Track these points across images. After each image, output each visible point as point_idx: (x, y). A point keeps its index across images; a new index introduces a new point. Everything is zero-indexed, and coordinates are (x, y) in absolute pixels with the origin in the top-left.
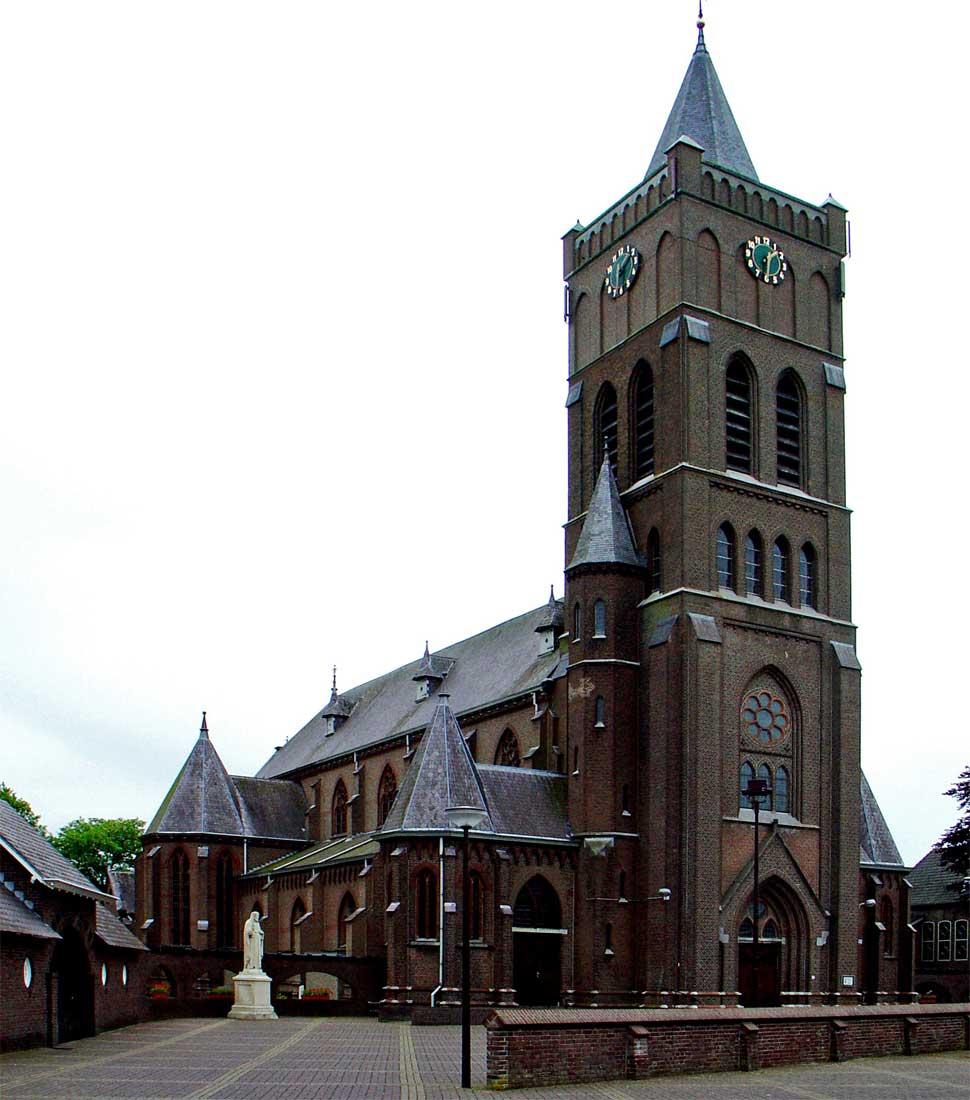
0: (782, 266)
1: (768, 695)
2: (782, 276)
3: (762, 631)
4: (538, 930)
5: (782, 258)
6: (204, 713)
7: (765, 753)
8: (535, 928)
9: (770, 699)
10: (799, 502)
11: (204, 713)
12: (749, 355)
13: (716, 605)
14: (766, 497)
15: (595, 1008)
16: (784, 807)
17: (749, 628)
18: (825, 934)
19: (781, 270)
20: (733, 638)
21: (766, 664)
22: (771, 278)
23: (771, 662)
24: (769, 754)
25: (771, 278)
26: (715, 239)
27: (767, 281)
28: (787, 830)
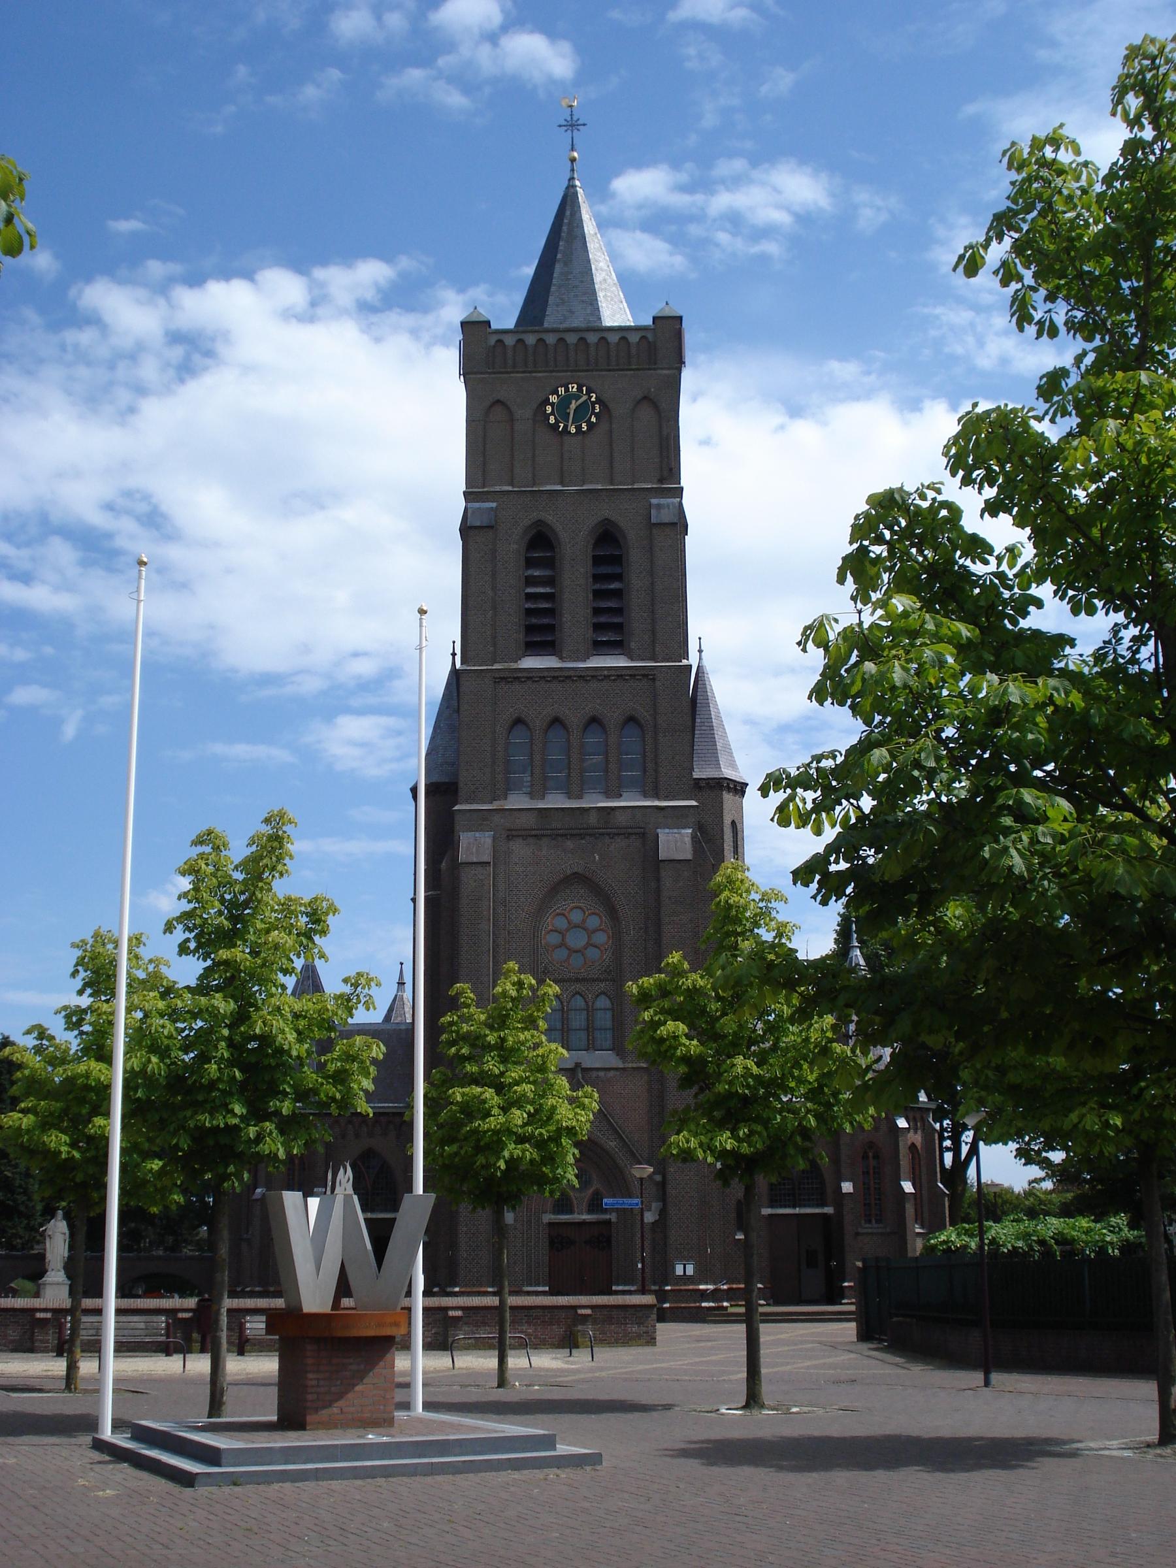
0: (594, 408)
1: (580, 908)
2: (593, 419)
3: (562, 835)
4: (797, 1211)
5: (593, 399)
6: (402, 964)
7: (577, 980)
8: (794, 1207)
9: (564, 915)
10: (613, 673)
11: (402, 964)
12: (549, 522)
13: (496, 818)
14: (569, 677)
15: (45, 1310)
16: (609, 1044)
17: (543, 835)
18: (656, 1206)
19: (593, 413)
20: (520, 850)
21: (569, 872)
22: (579, 428)
23: (576, 870)
24: (584, 980)
25: (579, 428)
26: (508, 408)
27: (573, 430)
28: (601, 1074)
